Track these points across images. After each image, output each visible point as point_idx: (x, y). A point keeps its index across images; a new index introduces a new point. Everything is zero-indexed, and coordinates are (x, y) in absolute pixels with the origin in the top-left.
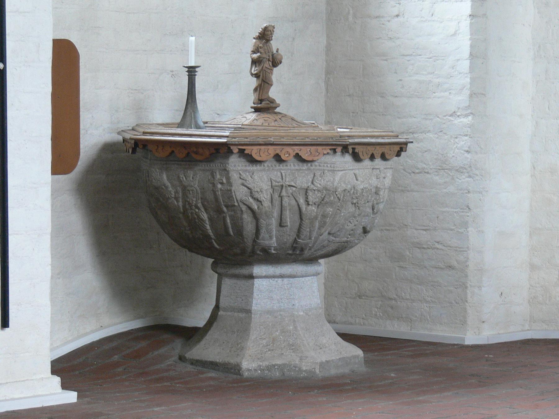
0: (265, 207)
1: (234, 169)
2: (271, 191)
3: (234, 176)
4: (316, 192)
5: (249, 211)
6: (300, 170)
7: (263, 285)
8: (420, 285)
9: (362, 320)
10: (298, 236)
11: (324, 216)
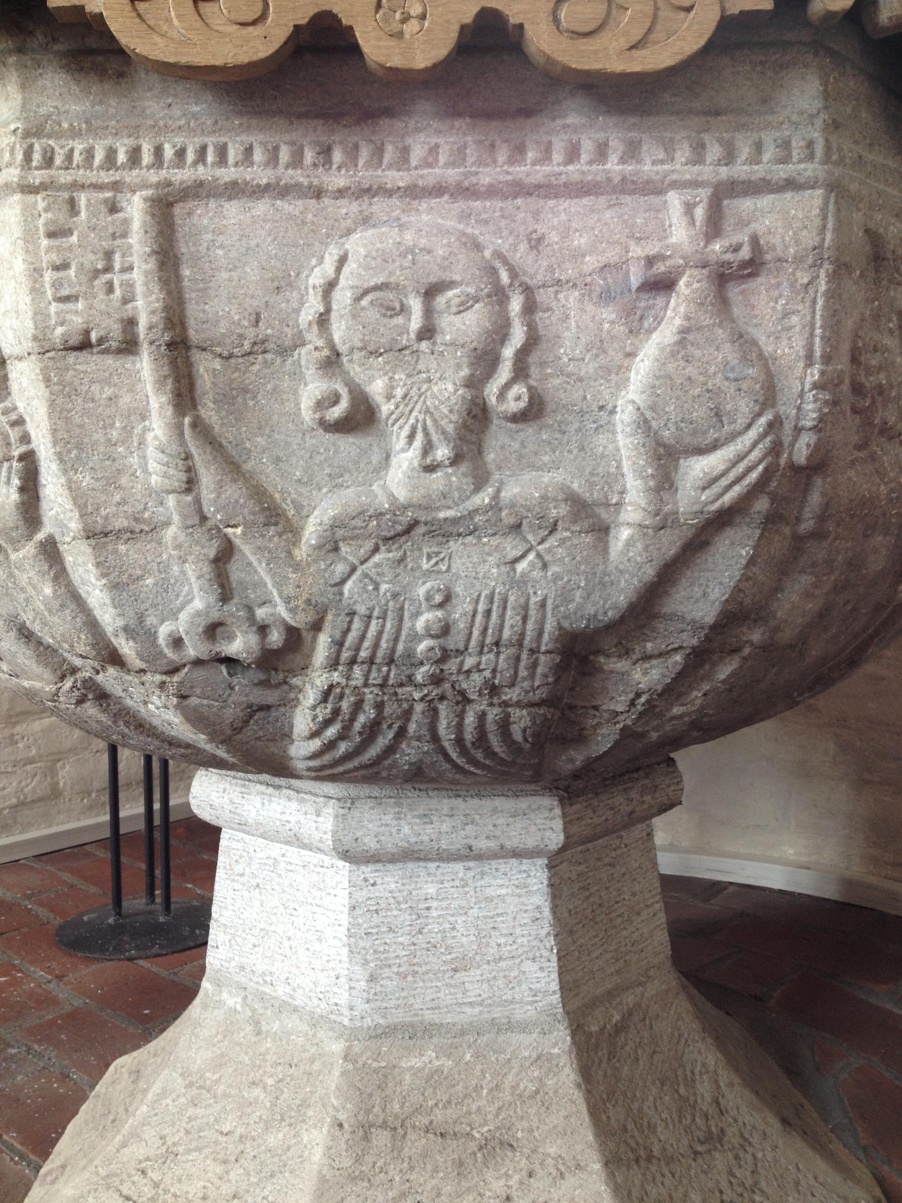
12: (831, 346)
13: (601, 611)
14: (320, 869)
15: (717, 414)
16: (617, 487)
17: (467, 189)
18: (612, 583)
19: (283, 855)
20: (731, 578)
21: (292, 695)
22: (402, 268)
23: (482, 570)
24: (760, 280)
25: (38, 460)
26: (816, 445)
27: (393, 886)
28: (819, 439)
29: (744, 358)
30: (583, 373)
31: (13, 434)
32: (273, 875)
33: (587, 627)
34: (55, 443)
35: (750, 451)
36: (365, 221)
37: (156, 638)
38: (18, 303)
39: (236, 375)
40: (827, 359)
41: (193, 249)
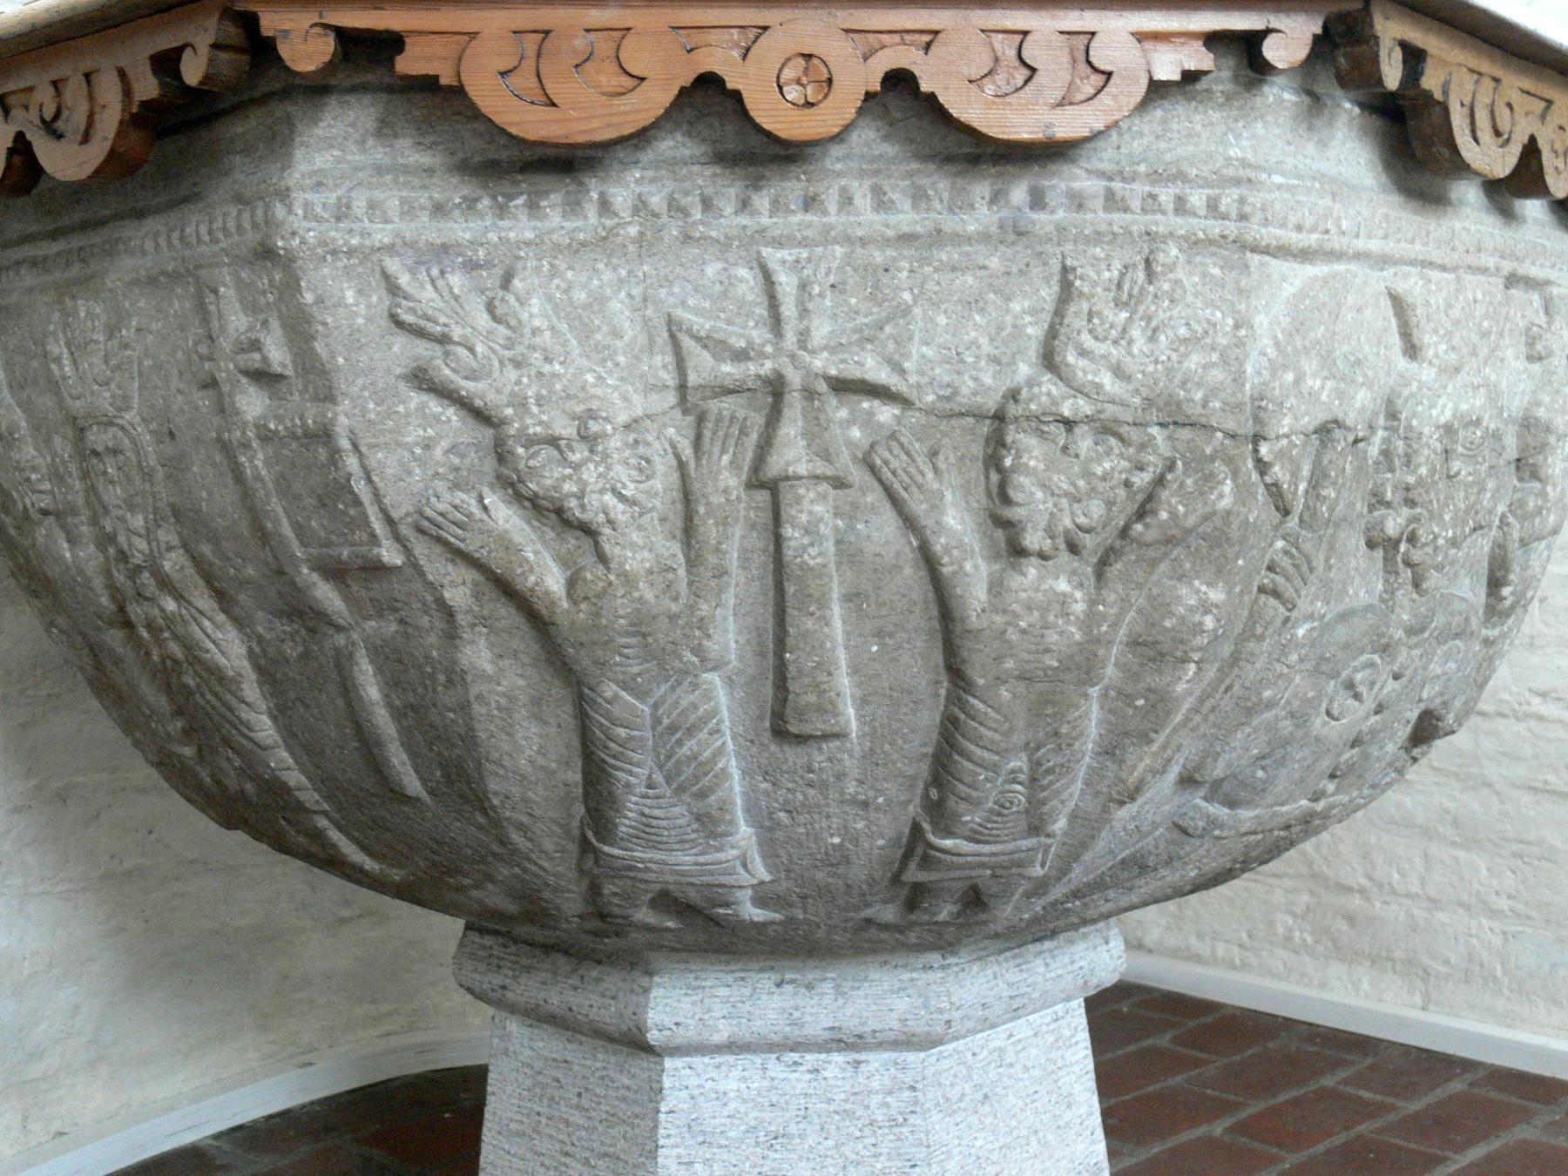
0: (628, 580)
1: (337, 235)
2: (677, 431)
3: (346, 304)
4: (1084, 443)
5: (506, 614)
6: (938, 237)
7: (721, 1097)
8: (1467, 849)
9: (1236, 949)
10: (938, 811)
11: (1155, 650)
19: (1011, 1036)
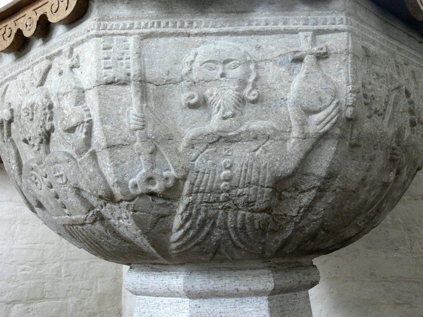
12: (355, 79)
13: (286, 170)
14: (178, 304)
15: (320, 100)
16: (289, 126)
17: (236, 33)
18: (289, 159)
19: (162, 301)
20: (330, 158)
21: (174, 210)
22: (216, 55)
23: (244, 154)
24: (330, 59)
25: (93, 122)
26: (353, 111)
27: (207, 308)
28: (354, 110)
29: (327, 82)
30: (275, 88)
31: (85, 114)
32: (157, 310)
33: (281, 176)
34: (100, 115)
35: (332, 112)
36: (204, 42)
37: (128, 186)
38: (91, 71)
39: (161, 91)
40: (353, 83)
41: (149, 53)
